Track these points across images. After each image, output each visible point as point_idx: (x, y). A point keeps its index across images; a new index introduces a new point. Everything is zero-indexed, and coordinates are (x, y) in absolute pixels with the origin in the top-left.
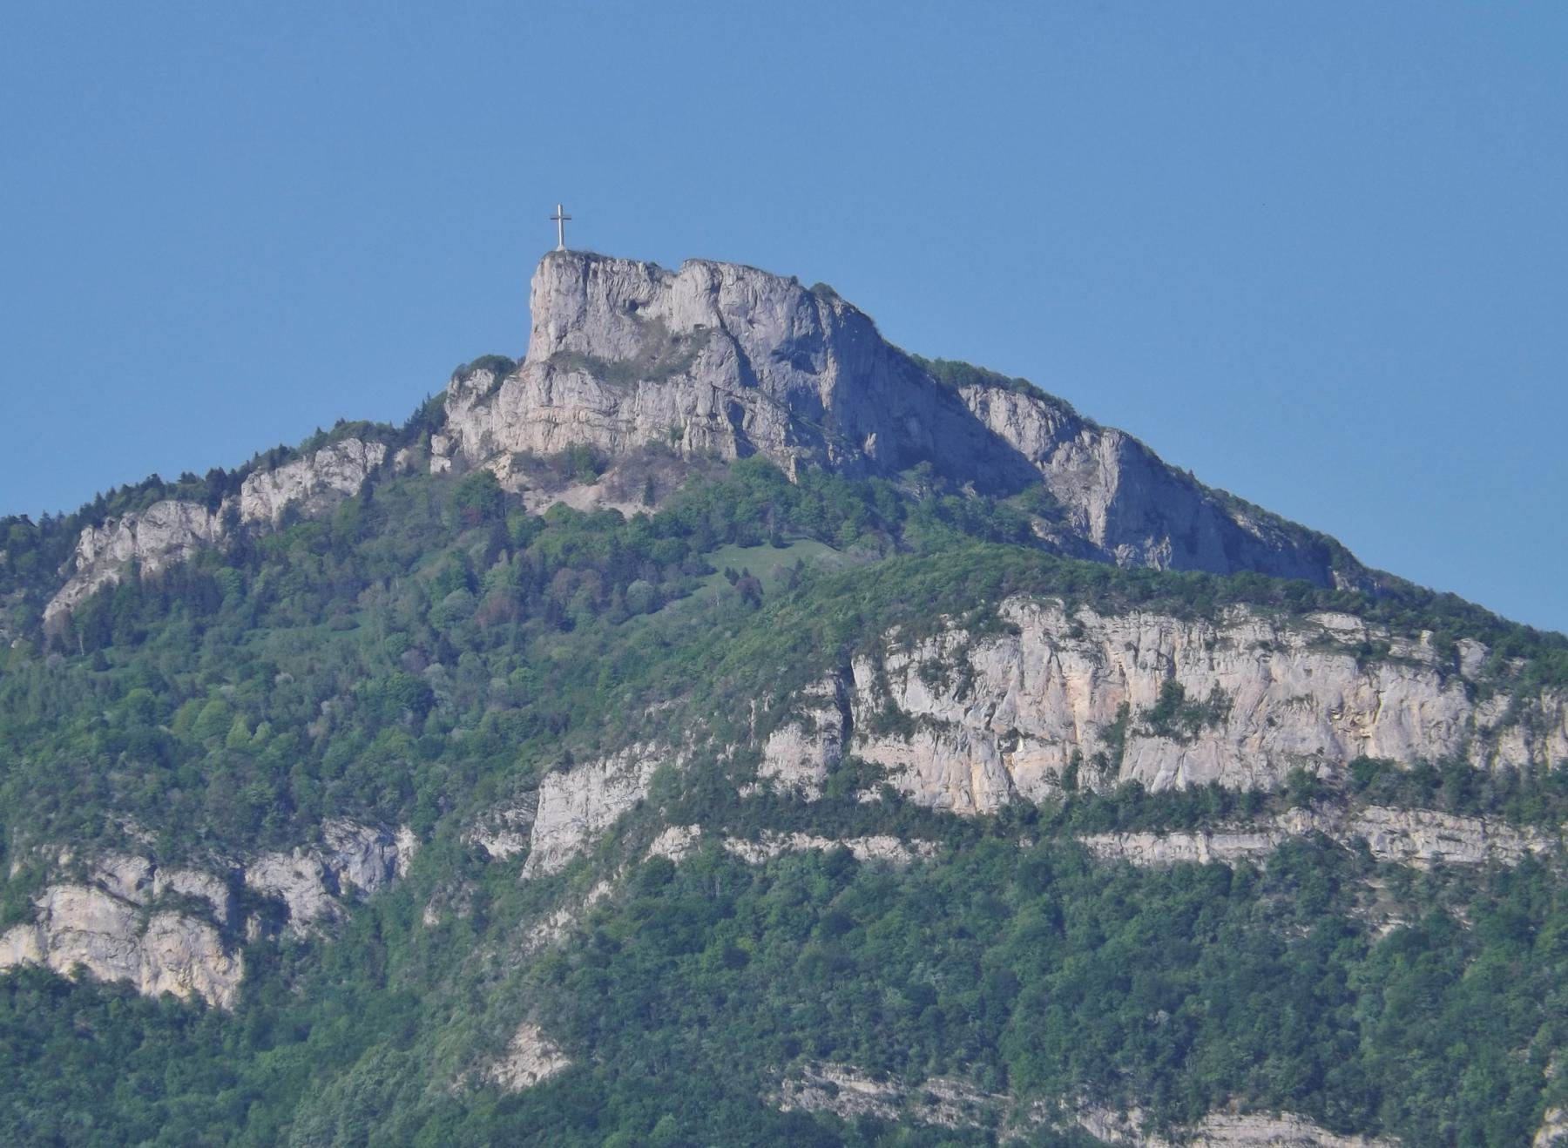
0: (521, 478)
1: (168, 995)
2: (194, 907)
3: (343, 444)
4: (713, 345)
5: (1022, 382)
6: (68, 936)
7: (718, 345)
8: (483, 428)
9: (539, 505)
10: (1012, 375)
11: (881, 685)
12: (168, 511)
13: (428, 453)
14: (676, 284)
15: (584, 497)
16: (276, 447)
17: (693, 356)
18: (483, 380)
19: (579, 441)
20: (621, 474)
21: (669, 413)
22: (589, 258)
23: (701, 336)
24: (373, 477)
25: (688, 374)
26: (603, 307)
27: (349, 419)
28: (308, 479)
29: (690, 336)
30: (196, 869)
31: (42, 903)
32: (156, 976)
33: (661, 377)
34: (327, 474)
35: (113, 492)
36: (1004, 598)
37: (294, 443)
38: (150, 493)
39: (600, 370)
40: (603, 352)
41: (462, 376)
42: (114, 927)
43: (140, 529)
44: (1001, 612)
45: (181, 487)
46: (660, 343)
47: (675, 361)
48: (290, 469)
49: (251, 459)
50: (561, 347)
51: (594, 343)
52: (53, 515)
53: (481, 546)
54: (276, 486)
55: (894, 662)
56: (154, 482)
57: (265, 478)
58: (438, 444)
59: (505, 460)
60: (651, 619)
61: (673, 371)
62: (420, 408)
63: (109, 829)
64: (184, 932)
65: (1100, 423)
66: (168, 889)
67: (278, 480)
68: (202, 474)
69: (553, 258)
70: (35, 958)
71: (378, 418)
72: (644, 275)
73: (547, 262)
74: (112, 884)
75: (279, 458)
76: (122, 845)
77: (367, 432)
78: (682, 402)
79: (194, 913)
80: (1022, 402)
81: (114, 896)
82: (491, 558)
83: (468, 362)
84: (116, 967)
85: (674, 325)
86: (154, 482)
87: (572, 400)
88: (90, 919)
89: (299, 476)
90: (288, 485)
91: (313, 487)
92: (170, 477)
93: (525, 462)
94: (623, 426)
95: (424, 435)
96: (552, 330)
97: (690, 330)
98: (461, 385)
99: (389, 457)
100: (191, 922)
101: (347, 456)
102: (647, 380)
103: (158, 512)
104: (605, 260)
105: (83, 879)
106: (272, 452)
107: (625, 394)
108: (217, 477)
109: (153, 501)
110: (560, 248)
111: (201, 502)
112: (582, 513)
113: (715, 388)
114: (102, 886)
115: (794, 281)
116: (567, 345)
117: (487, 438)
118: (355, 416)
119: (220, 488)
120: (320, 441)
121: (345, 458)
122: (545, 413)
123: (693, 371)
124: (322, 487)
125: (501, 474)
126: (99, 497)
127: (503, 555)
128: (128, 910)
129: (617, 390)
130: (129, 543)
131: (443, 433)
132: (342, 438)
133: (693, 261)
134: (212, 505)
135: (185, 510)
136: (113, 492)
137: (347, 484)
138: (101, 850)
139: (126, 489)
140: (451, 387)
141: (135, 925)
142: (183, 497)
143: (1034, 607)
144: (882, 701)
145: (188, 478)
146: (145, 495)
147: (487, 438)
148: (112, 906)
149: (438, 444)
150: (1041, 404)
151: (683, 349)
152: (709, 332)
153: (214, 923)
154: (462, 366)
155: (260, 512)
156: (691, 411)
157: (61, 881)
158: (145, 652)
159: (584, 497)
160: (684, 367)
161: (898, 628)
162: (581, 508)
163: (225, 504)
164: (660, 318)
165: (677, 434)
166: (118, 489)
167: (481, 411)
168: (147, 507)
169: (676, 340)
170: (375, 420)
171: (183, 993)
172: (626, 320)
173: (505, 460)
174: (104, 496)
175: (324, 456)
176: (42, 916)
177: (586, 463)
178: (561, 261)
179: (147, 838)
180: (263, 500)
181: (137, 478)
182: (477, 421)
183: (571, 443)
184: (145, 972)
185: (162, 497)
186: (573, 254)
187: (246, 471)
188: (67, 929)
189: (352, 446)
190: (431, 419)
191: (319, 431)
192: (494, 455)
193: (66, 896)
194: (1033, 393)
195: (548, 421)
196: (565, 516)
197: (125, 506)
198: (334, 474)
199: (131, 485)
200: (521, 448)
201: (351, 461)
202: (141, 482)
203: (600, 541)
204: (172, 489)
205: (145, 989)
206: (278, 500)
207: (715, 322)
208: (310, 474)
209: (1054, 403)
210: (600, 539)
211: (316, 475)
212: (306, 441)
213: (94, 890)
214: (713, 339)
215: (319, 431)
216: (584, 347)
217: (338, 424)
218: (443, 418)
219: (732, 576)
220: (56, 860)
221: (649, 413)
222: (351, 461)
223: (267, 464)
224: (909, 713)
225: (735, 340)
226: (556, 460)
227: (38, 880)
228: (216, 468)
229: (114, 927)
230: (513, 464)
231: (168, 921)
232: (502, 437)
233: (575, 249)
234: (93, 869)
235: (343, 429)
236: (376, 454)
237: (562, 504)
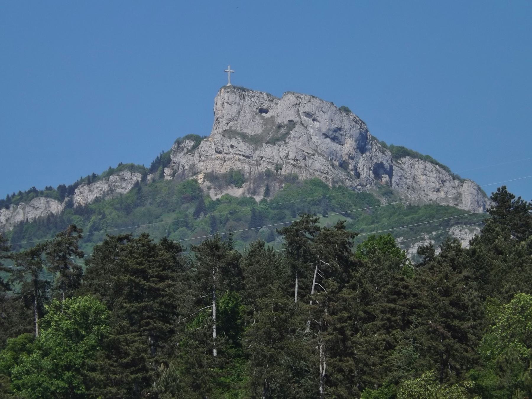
0: (207, 183)
3: (121, 173)
9: (214, 195)
10: (424, 154)
12: (41, 202)
15: (237, 192)
16: (91, 174)
17: (287, 134)
18: (190, 144)
20: (254, 183)
25: (285, 141)
27: (124, 163)
28: (106, 187)
29: (286, 125)
34: (114, 186)
35: (14, 195)
36: (452, 226)
38: (31, 194)
40: (250, 132)
41: (179, 142)
44: (450, 233)
45: (45, 192)
46: (272, 128)
47: (279, 135)
48: (97, 184)
49: (79, 179)
50: (228, 128)
53: (192, 210)
54: (90, 191)
56: (34, 190)
57: (86, 188)
59: (201, 176)
62: (159, 156)
67: (92, 189)
68: (55, 187)
69: (225, 89)
73: (222, 90)
75: (92, 179)
77: (132, 168)
80: (429, 165)
82: (197, 214)
83: (183, 135)
85: (279, 120)
86: (34, 190)
89: (101, 186)
90: (96, 191)
91: (108, 191)
92: (40, 188)
93: (211, 177)
95: (161, 168)
97: (286, 122)
98: (178, 146)
101: (124, 178)
102: (267, 143)
103: (36, 202)
104: (248, 90)
106: (89, 177)
108: (62, 188)
109: (33, 198)
110: (229, 84)
112: (237, 198)
116: (230, 127)
118: (127, 161)
119: (65, 192)
120: (111, 172)
121: (123, 179)
123: (287, 140)
124: (111, 191)
125: (200, 181)
126: (8, 196)
127: (202, 214)
131: (169, 167)
132: (121, 170)
133: (288, 93)
134: (60, 199)
136: (14, 195)
137: (123, 190)
139: (20, 193)
140: (174, 147)
142: (47, 196)
143: (466, 230)
145: (49, 189)
146: (34, 193)
147: (192, 167)
150: (437, 167)
151: (283, 130)
154: (179, 138)
155: (83, 203)
159: (237, 192)
161: (402, 238)
162: (237, 196)
163: (66, 199)
166: (16, 194)
168: (30, 200)
169: (279, 127)
170: (136, 164)
173: (201, 176)
174: (10, 196)
177: (235, 179)
178: (229, 90)
180: (83, 197)
183: (231, 169)
185: (37, 196)
186: (234, 88)
187: (76, 186)
189: (127, 174)
190: (164, 161)
191: (110, 168)
192: (196, 173)
195: (221, 159)
196: (229, 199)
197: (21, 200)
198: (117, 186)
200: (209, 170)
201: (125, 180)
202: (27, 191)
203: (247, 209)
204: (42, 193)
206: (91, 198)
210: (247, 209)
211: (109, 186)
212: (104, 172)
214: (297, 126)
215: (110, 168)
216: (238, 128)
217: (119, 165)
218: (169, 160)
222: (125, 180)
223: (87, 182)
226: (224, 176)
228: (62, 184)
230: (204, 178)
233: (236, 85)
235: (122, 167)
236: (138, 177)
237: (227, 194)
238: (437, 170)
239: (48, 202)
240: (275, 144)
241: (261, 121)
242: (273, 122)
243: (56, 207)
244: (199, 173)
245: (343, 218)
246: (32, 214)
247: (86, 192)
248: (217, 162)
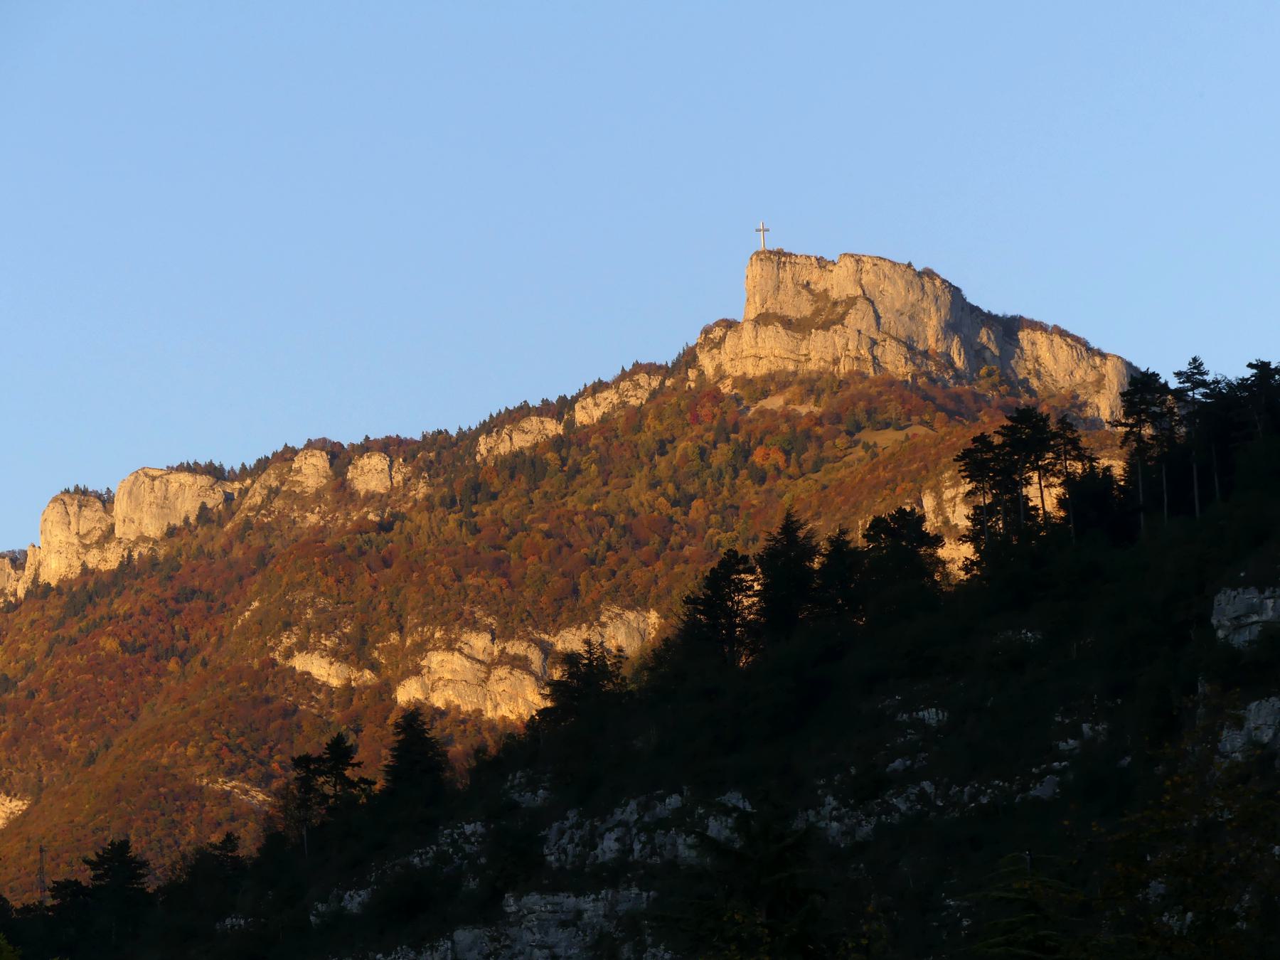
1: (504, 718)
2: (520, 663)
3: (636, 377)
4: (858, 306)
5: (1056, 327)
6: (441, 683)
7: (862, 305)
8: (717, 362)
10: (1050, 322)
11: (939, 509)
12: (533, 423)
13: (686, 379)
14: (836, 269)
17: (846, 313)
19: (774, 368)
21: (831, 350)
22: (780, 253)
23: (851, 302)
24: (654, 394)
26: (790, 285)
30: (520, 638)
31: (424, 663)
32: (496, 707)
33: (826, 326)
37: (608, 378)
39: (787, 323)
40: (791, 313)
42: (469, 677)
43: (515, 436)
47: (834, 317)
48: (605, 394)
51: (784, 306)
52: (465, 428)
54: (596, 405)
55: (948, 494)
57: (589, 400)
58: (692, 374)
59: (729, 382)
60: (815, 476)
61: (834, 323)
63: (466, 615)
64: (512, 679)
65: (1105, 350)
66: (503, 651)
70: (420, 696)
71: (660, 361)
72: (815, 264)
74: (466, 650)
76: (475, 626)
77: (651, 369)
78: (840, 342)
79: (519, 667)
80: (1057, 339)
81: (468, 657)
84: (471, 702)
85: (834, 295)
87: (770, 343)
88: (454, 671)
89: (610, 396)
90: (603, 404)
94: (803, 359)
96: (757, 299)
99: (662, 383)
100: (517, 673)
102: (817, 329)
103: (525, 425)
105: (450, 647)
107: (804, 338)
108: (562, 399)
111: (552, 417)
113: (859, 332)
114: (460, 651)
115: (910, 265)
117: (719, 368)
120: (624, 375)
121: (637, 386)
122: (753, 352)
128: (477, 666)
129: (798, 336)
130: (508, 444)
134: (559, 418)
135: (542, 422)
138: (461, 628)
141: (483, 675)
144: (940, 518)
145: (545, 402)
146: (524, 411)
147: (719, 368)
148: (468, 664)
149: (692, 374)
151: (840, 310)
152: (856, 298)
153: (531, 673)
156: (846, 347)
157: (436, 649)
158: (496, 505)
159: (775, 403)
160: (841, 320)
164: (826, 290)
165: (836, 361)
167: (715, 351)
169: (835, 304)
171: (513, 717)
172: (804, 292)
175: (625, 385)
176: (425, 670)
179: (490, 620)
180: (585, 415)
181: (513, 404)
182: (713, 358)
184: (489, 705)
186: (770, 252)
188: (440, 679)
189: (642, 378)
190: (688, 358)
193: (439, 658)
194: (1063, 334)
199: (511, 408)
200: (739, 374)
201: (641, 387)
205: (489, 714)
206: (597, 413)
207: (860, 292)
208: (616, 396)
209: (1077, 339)
213: (456, 654)
218: (695, 358)
219: (867, 447)
220: (433, 635)
221: (820, 351)
222: (641, 387)
224: (956, 525)
225: (872, 303)
227: (422, 648)
229: (469, 677)
231: (501, 672)
232: (728, 367)
234: (456, 640)
235: (638, 368)
238: (1069, 345)
239: (542, 422)
240: (828, 330)
241: (810, 297)
242: (827, 297)
243: (553, 428)
244: (727, 377)
245: (200, 657)
246: (521, 441)
247: (591, 406)
248: (750, 360)
